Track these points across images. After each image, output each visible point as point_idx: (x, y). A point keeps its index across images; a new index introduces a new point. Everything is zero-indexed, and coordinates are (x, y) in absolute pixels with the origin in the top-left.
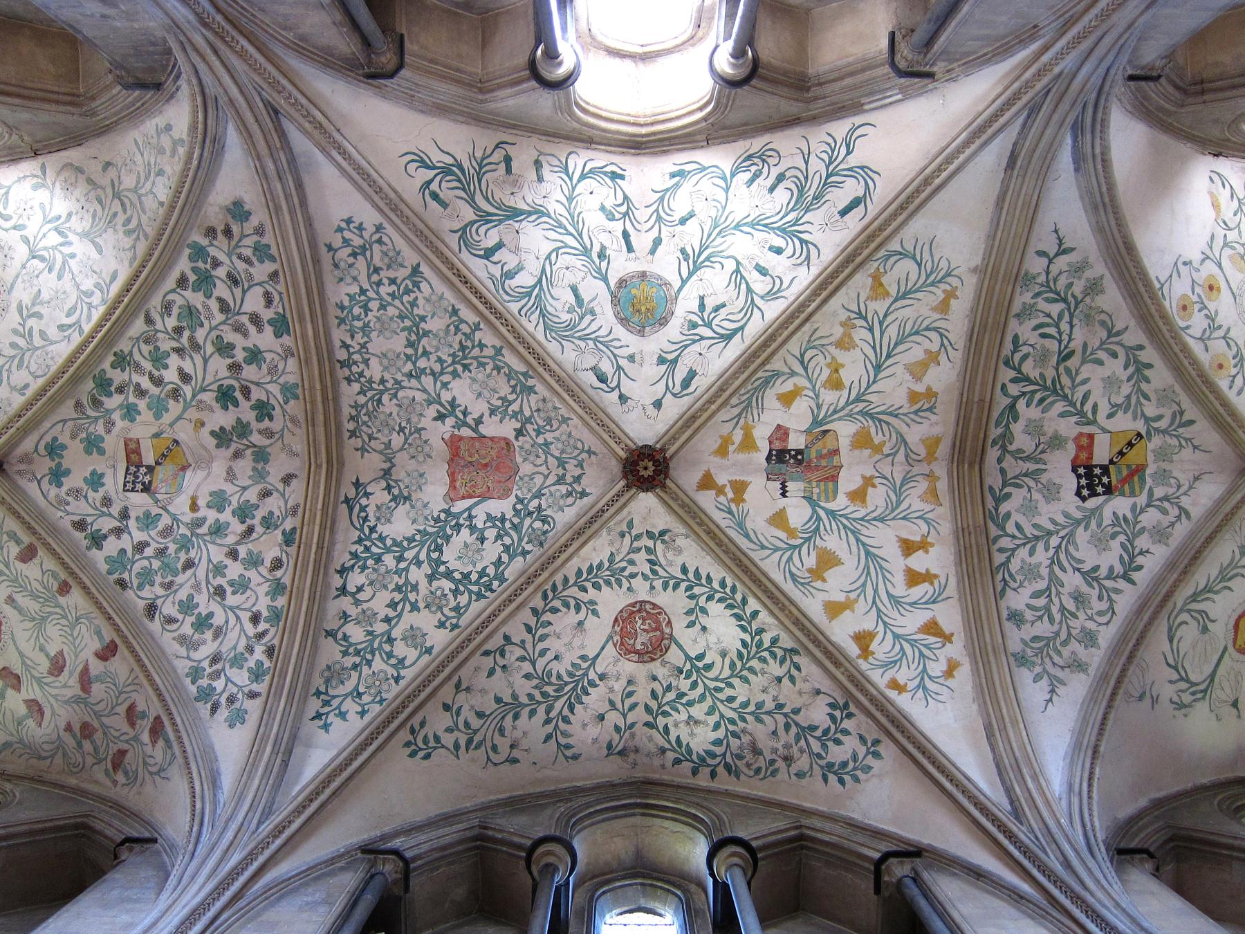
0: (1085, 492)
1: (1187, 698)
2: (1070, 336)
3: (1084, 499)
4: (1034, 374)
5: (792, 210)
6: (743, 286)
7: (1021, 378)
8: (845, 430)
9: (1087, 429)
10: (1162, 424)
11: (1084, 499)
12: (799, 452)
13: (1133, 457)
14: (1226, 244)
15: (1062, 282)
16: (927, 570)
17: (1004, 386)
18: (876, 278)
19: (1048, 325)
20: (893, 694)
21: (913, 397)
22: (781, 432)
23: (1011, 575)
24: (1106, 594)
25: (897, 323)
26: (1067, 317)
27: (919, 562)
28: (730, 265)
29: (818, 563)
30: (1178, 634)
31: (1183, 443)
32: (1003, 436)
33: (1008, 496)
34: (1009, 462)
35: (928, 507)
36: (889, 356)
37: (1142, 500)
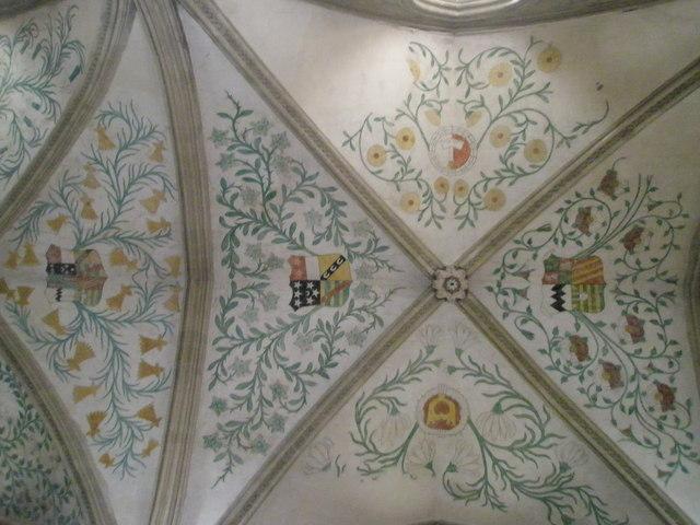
0: (298, 303)
1: (375, 466)
2: (269, 179)
3: (296, 308)
4: (246, 210)
5: (45, 74)
6: (18, 134)
7: (235, 213)
8: (104, 251)
9: (298, 253)
10: (361, 249)
11: (296, 308)
12: (72, 266)
13: (339, 274)
14: (423, 103)
15: (251, 138)
16: (157, 365)
17: (221, 219)
18: (101, 131)
19: (250, 171)
20: (101, 467)
21: (152, 226)
22: (54, 250)
23: (223, 370)
24: (302, 387)
25: (127, 167)
26: (263, 165)
27: (152, 358)
28: (10, 116)
29: (77, 354)
30: (366, 417)
31: (380, 264)
32: (230, 257)
33: (235, 304)
34: (238, 277)
35: (167, 312)
36: (126, 193)
37: (344, 309)
